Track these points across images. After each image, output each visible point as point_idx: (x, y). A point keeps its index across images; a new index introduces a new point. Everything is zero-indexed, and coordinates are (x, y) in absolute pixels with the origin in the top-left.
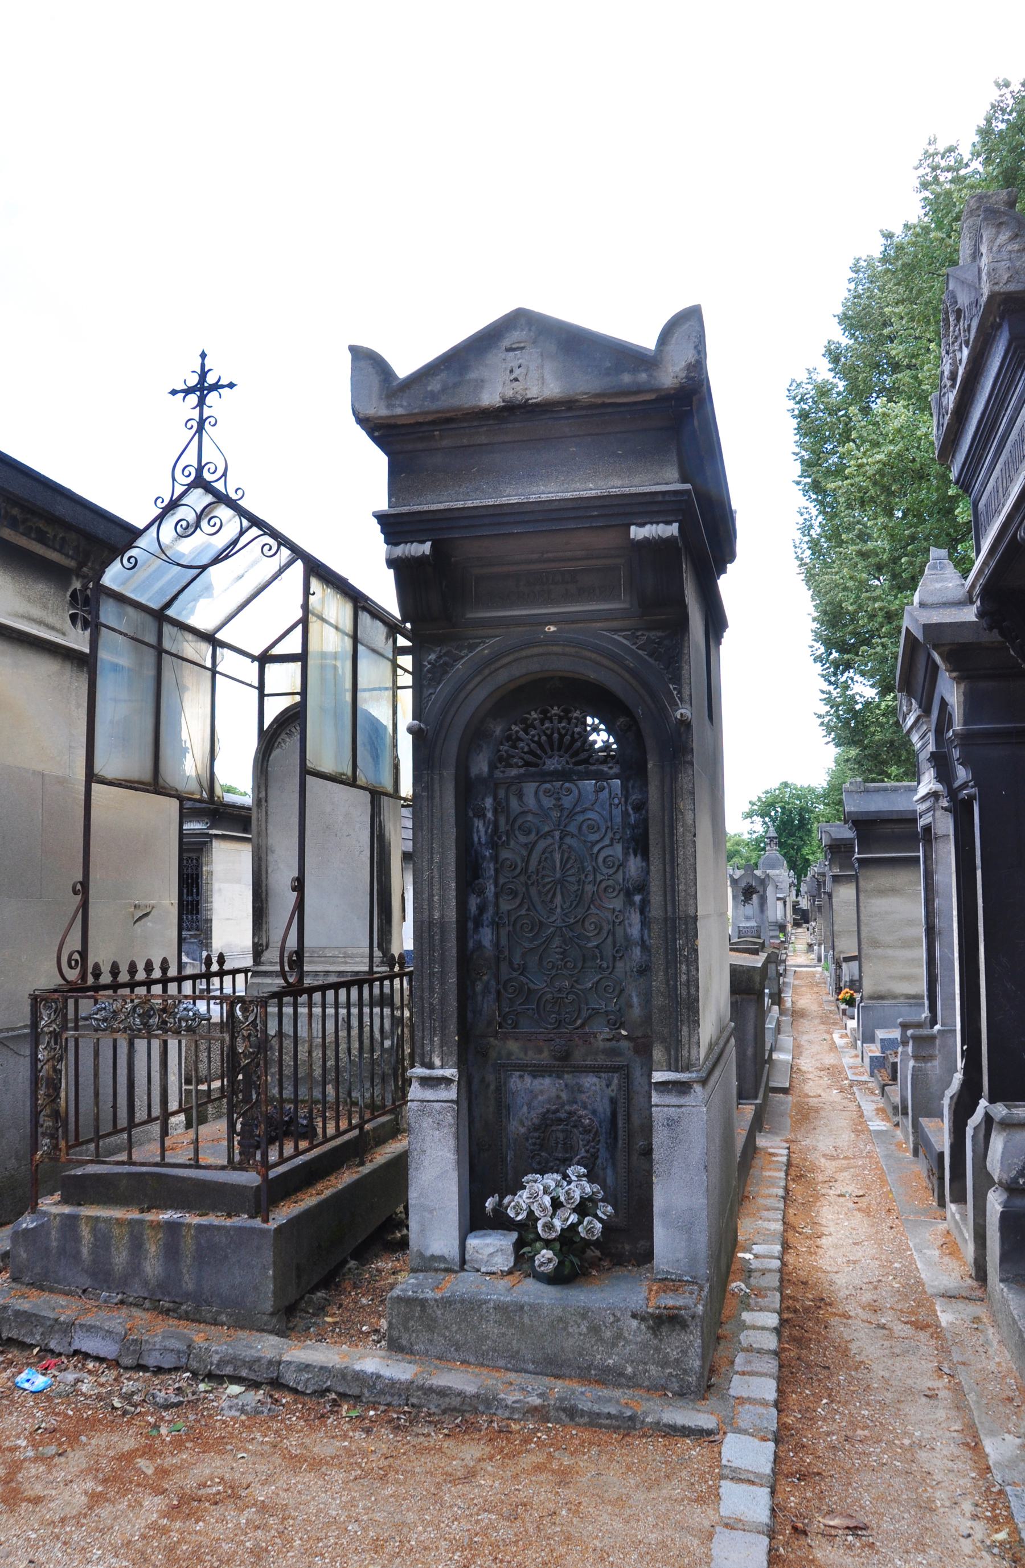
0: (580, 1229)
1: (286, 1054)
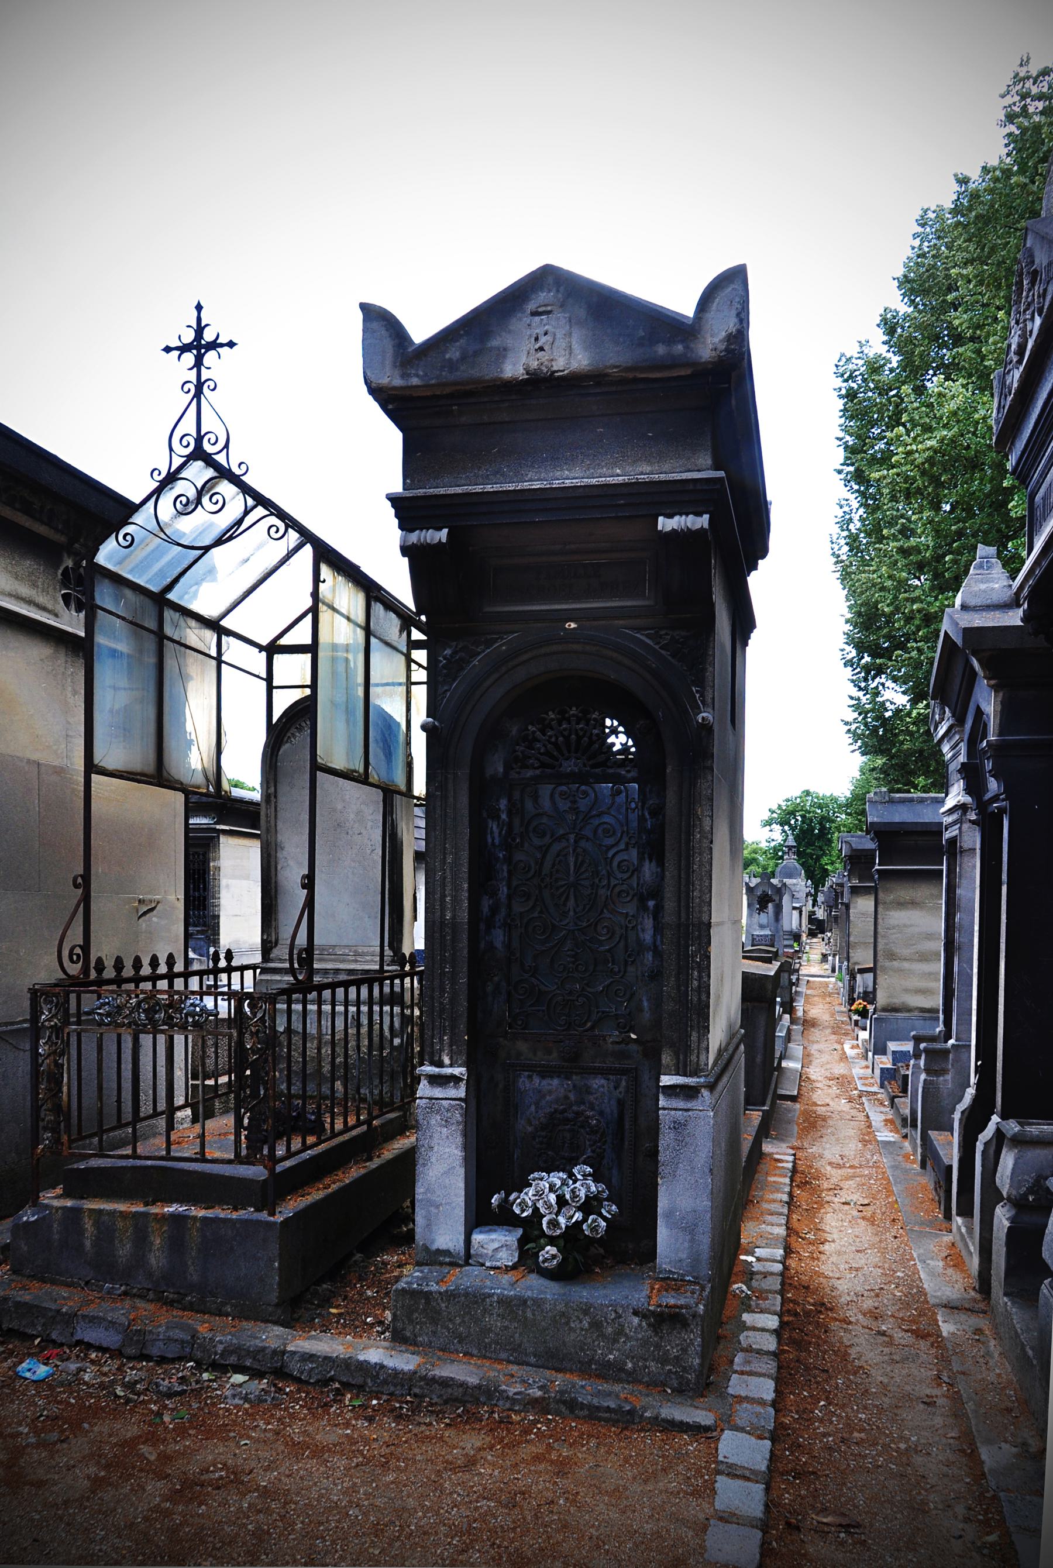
0: (585, 1227)
1: (295, 1050)
